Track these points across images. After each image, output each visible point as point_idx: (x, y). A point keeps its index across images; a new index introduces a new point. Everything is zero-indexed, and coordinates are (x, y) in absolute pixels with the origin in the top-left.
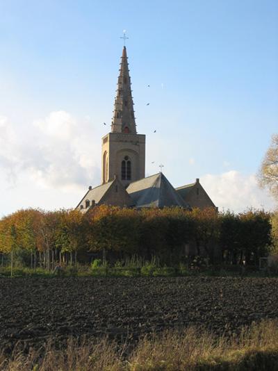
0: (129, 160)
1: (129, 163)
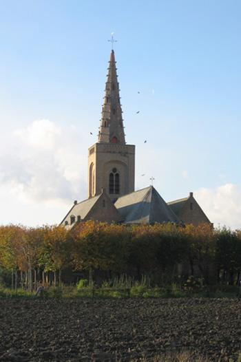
0: (117, 172)
1: (117, 175)
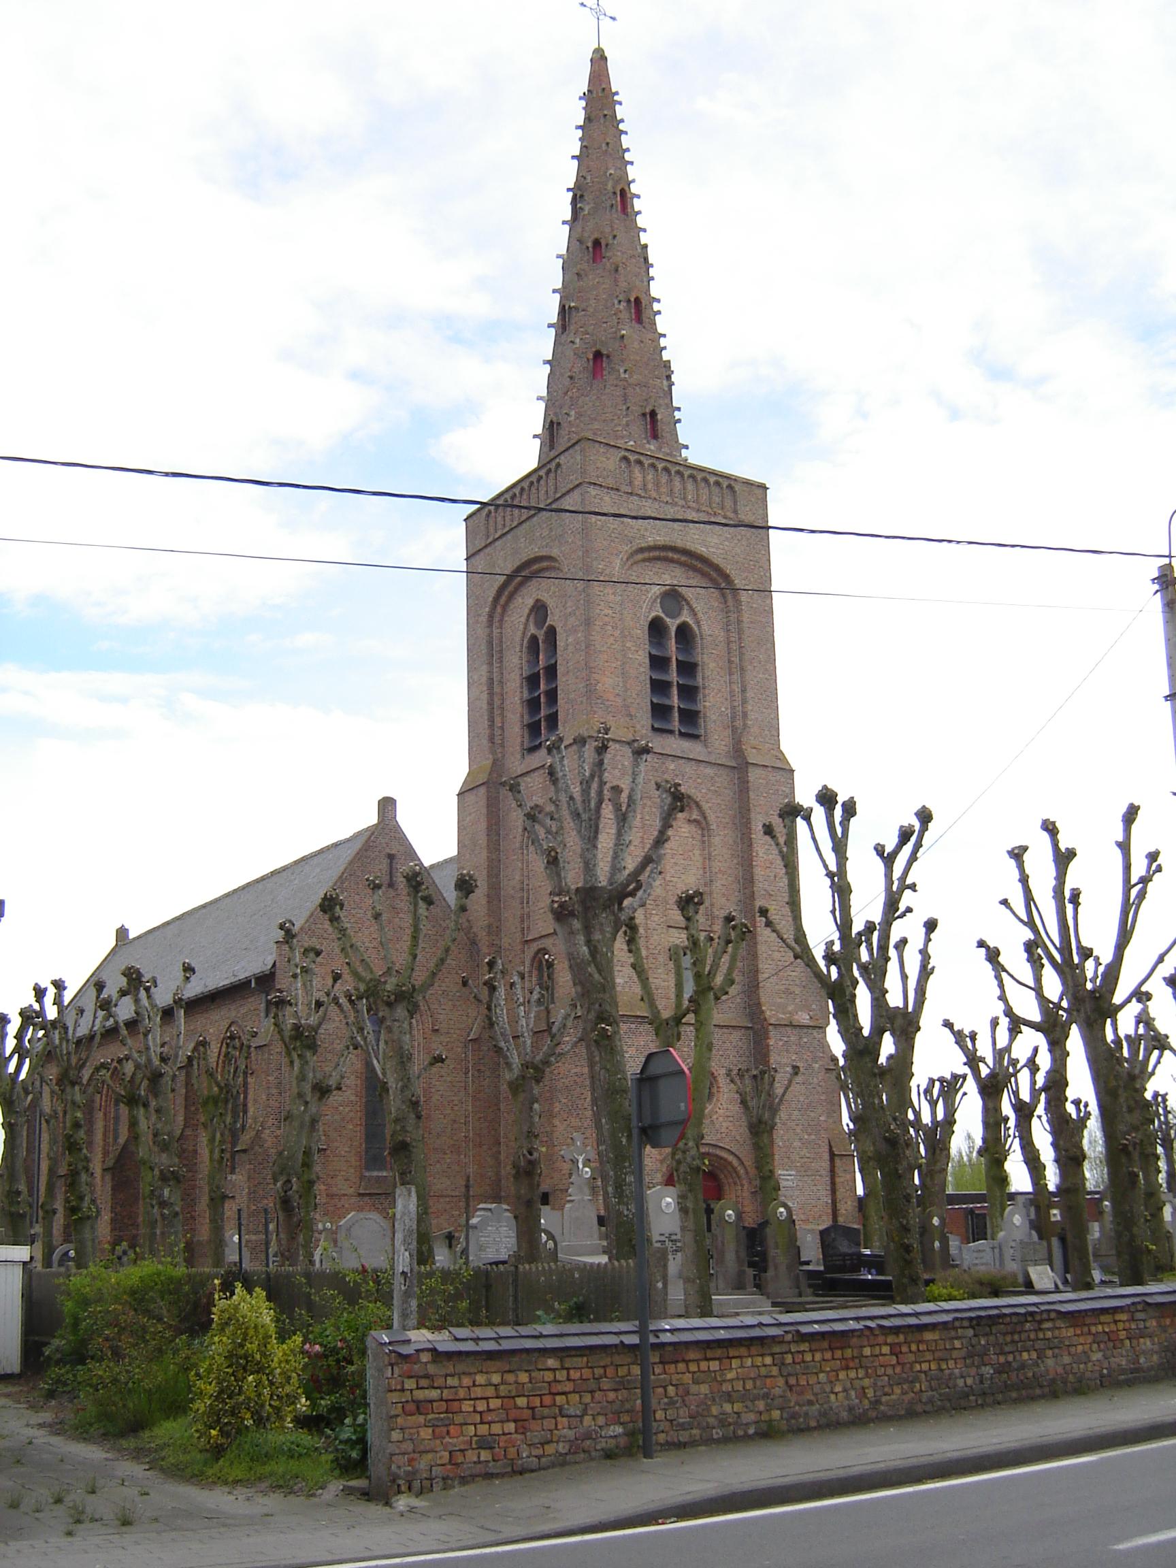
0: (686, 617)
1: (684, 633)
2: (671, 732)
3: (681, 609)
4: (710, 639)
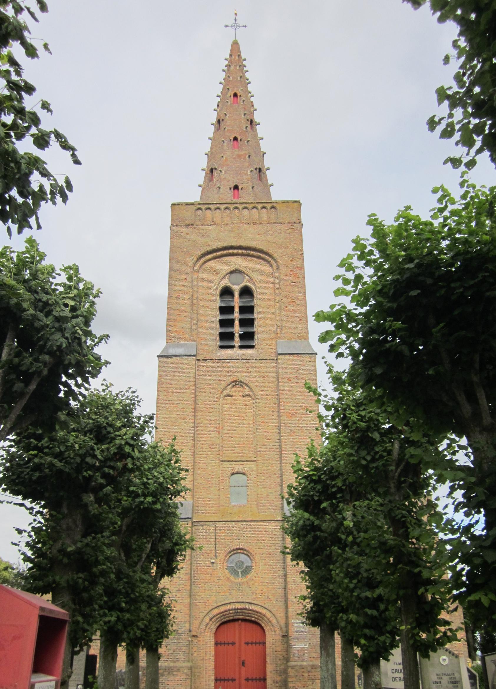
0: (247, 282)
2: (233, 347)
3: (244, 279)
4: (262, 291)
